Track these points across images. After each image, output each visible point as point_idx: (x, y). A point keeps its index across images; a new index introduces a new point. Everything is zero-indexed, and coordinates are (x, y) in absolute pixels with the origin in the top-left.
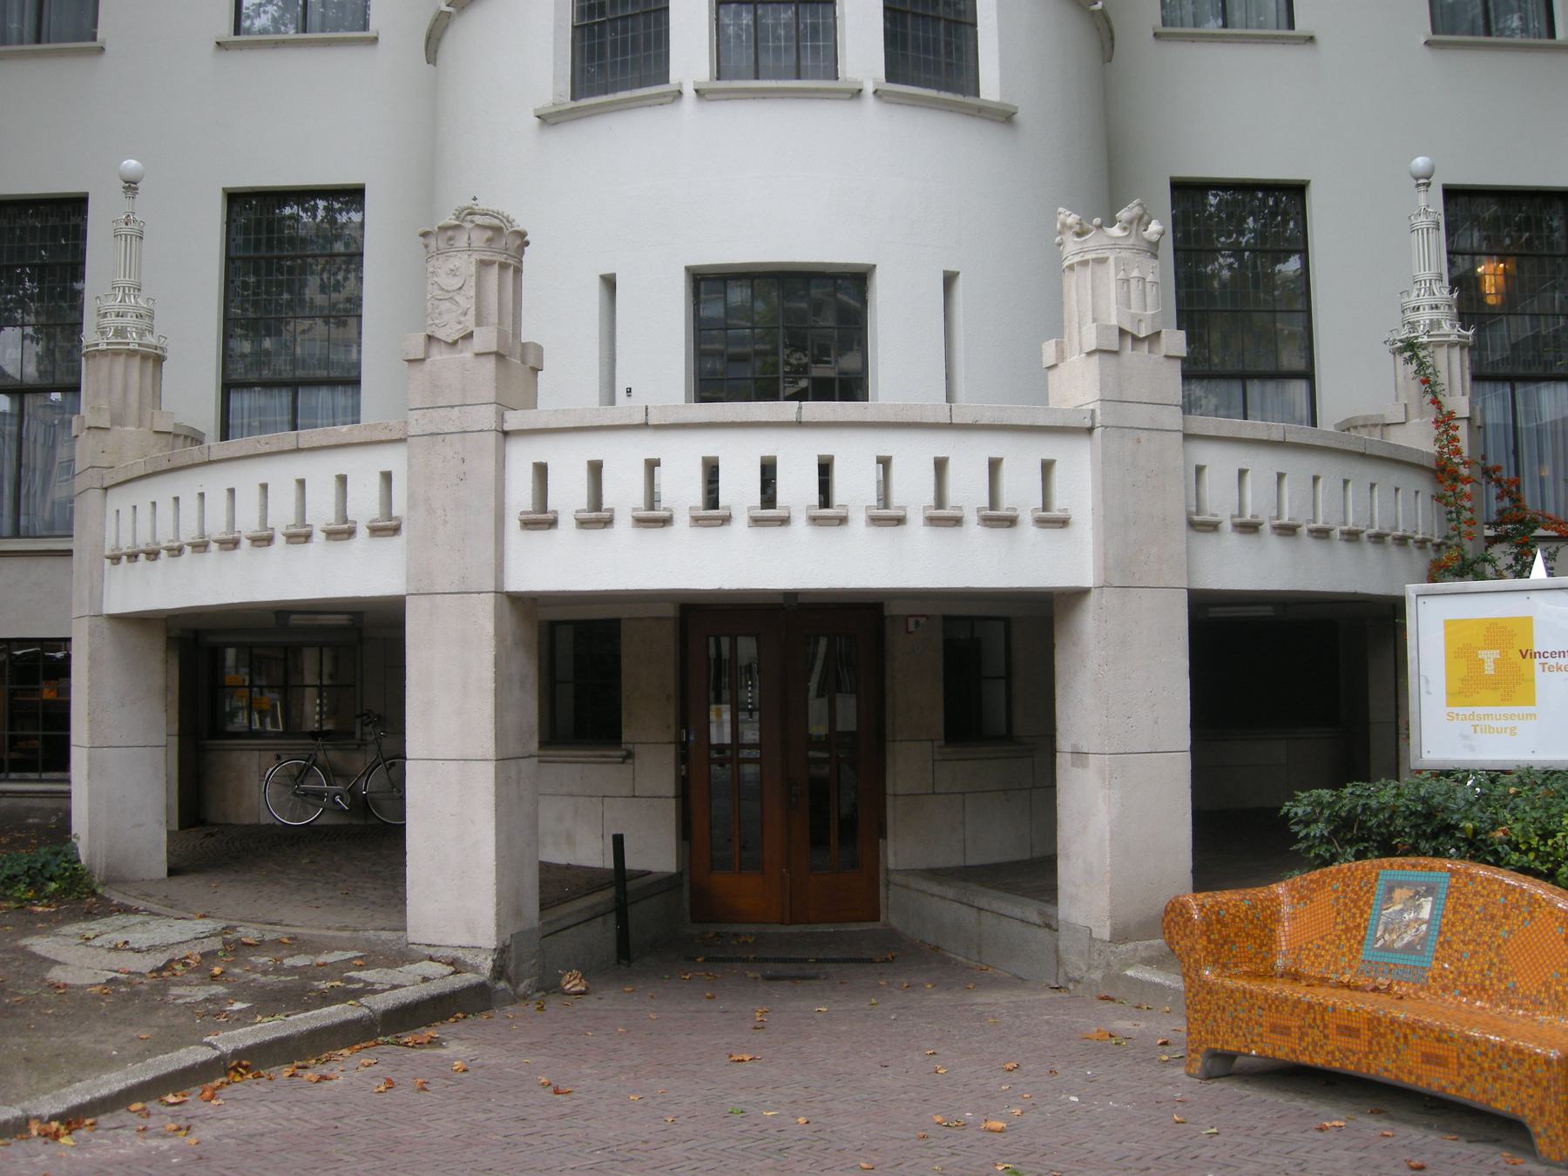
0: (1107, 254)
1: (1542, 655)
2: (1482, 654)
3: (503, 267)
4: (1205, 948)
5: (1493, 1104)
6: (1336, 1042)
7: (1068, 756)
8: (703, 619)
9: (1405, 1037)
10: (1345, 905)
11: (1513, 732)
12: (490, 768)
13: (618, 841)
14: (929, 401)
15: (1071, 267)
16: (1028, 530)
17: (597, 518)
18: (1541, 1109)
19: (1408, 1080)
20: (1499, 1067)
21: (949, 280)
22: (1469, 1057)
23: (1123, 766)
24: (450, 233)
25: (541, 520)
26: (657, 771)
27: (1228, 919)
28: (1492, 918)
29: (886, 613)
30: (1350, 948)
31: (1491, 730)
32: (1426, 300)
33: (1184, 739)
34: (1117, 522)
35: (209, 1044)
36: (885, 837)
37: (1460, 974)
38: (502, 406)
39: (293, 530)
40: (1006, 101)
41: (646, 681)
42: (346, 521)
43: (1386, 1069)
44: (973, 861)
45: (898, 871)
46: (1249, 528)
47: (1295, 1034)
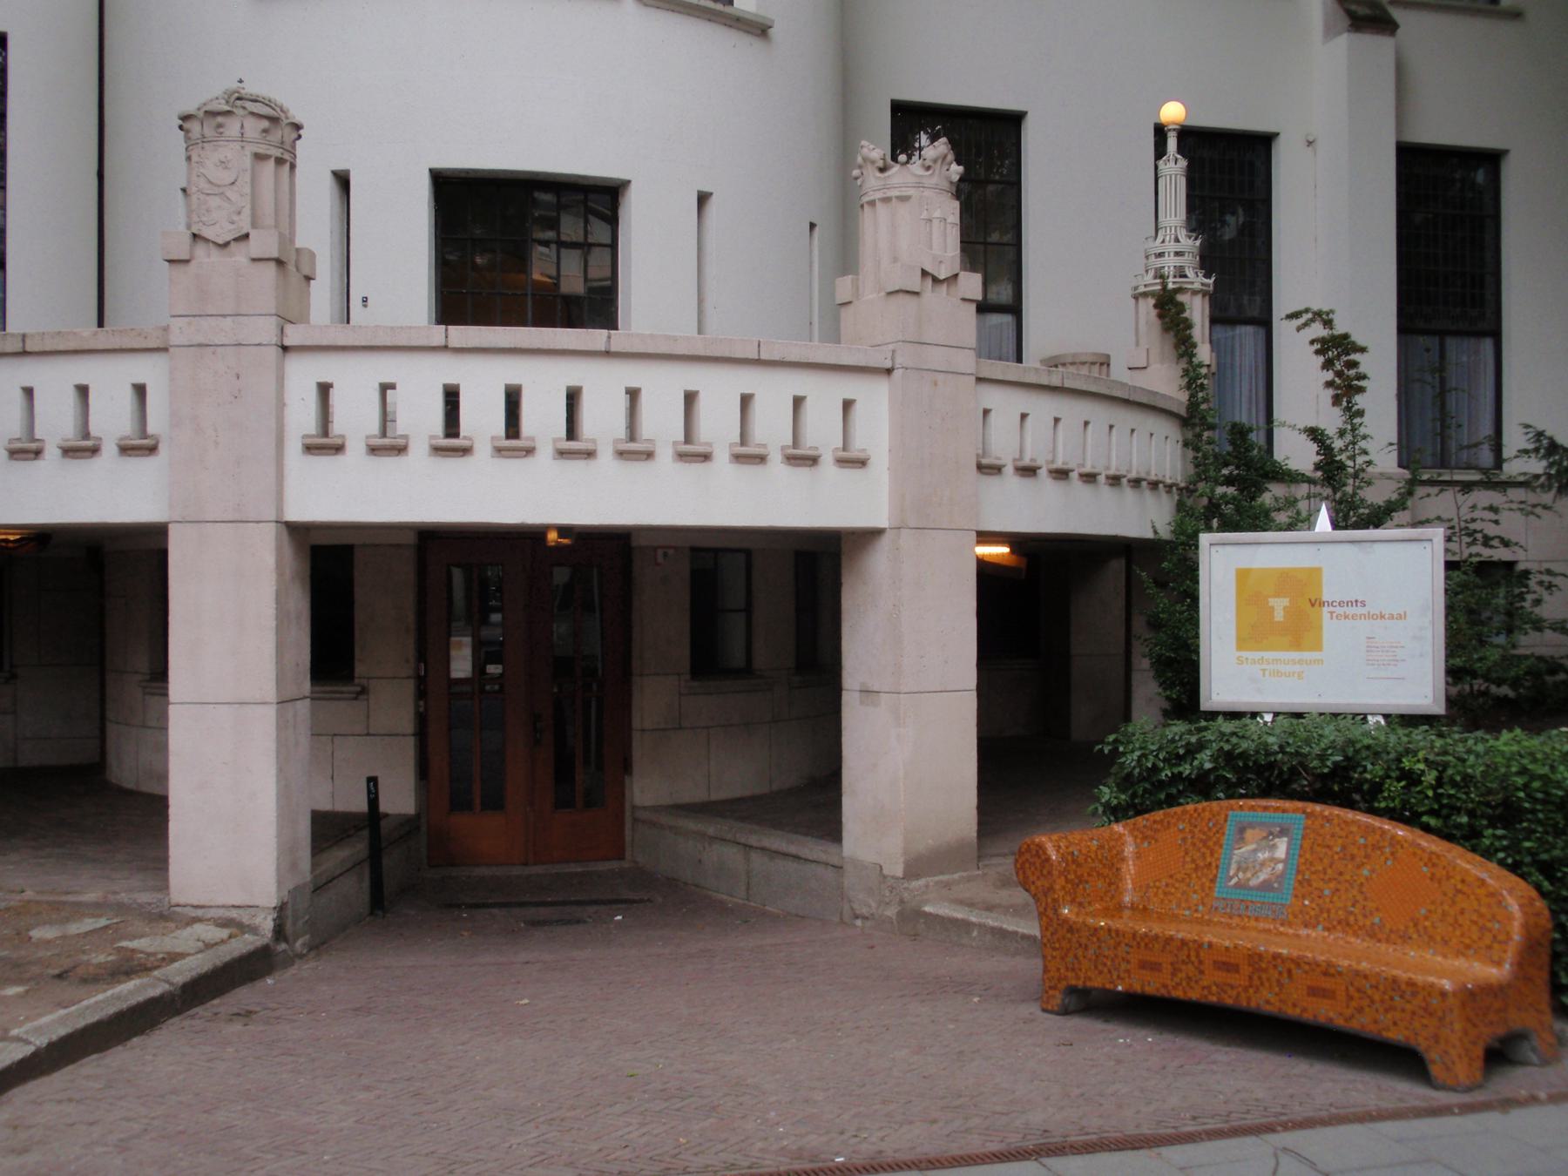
0: (911, 192)
1: (1331, 604)
2: (1272, 602)
3: (280, 161)
4: (1063, 888)
5: (1385, 1034)
6: (1212, 977)
7: (857, 695)
8: (436, 546)
9: (1289, 971)
10: (1194, 844)
11: (1300, 676)
12: (270, 713)
13: (373, 781)
14: (679, 327)
15: (872, 203)
16: (776, 465)
18: (1436, 1039)
19: (1292, 1012)
20: (1392, 999)
21: (703, 199)
22: (1359, 990)
23: (911, 708)
24: (220, 119)
25: (325, 445)
26: (394, 707)
27: (1081, 859)
28: (1353, 857)
29: (634, 544)
30: (1203, 886)
31: (1278, 674)
32: (1171, 247)
33: (968, 675)
35: (18, 1039)
36: (630, 774)
37: (1321, 911)
38: (285, 320)
39: (19, 445)
40: (762, 13)
41: (382, 610)
42: (86, 435)
43: (1268, 1002)
44: (715, 797)
45: (645, 808)
46: (1028, 471)
47: (1167, 969)
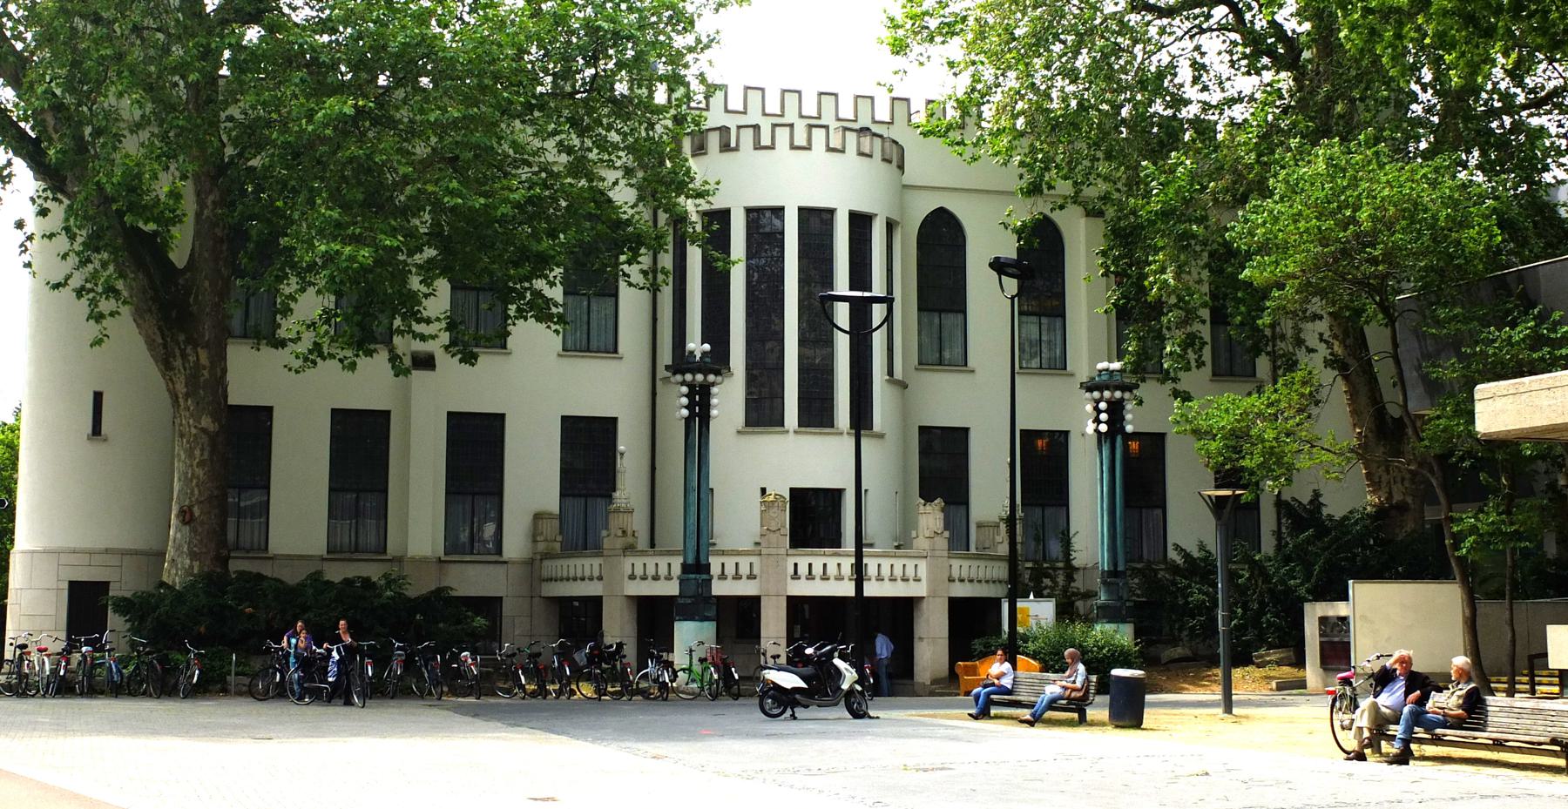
17: (810, 576)
34: (932, 581)
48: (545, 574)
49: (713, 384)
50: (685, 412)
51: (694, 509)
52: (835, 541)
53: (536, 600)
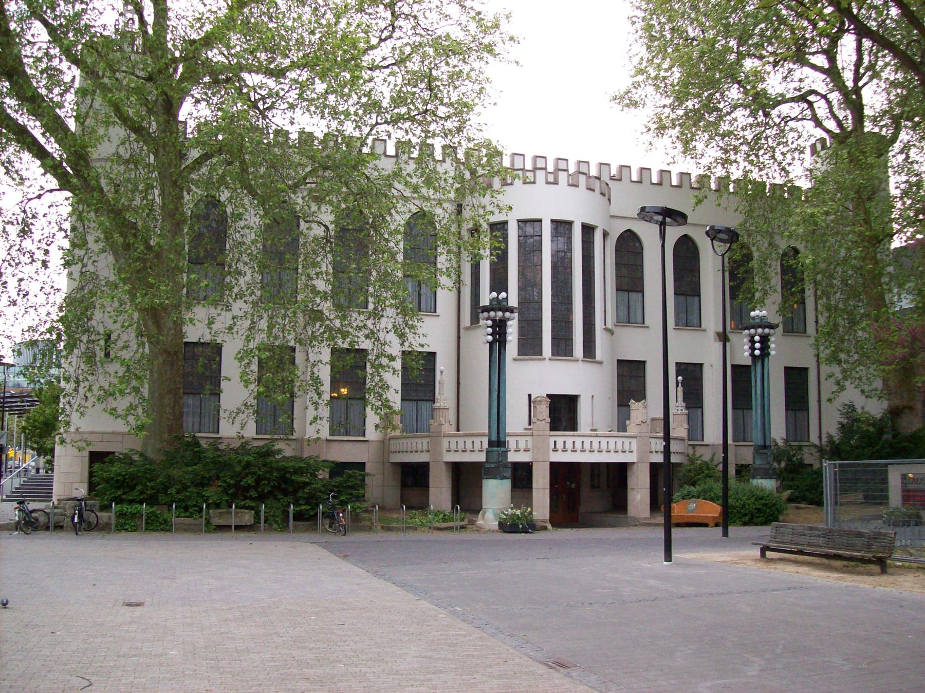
48: (392, 449)
49: (508, 319)
50: (490, 338)
51: (495, 403)
52: (332, 434)
53: (387, 464)
